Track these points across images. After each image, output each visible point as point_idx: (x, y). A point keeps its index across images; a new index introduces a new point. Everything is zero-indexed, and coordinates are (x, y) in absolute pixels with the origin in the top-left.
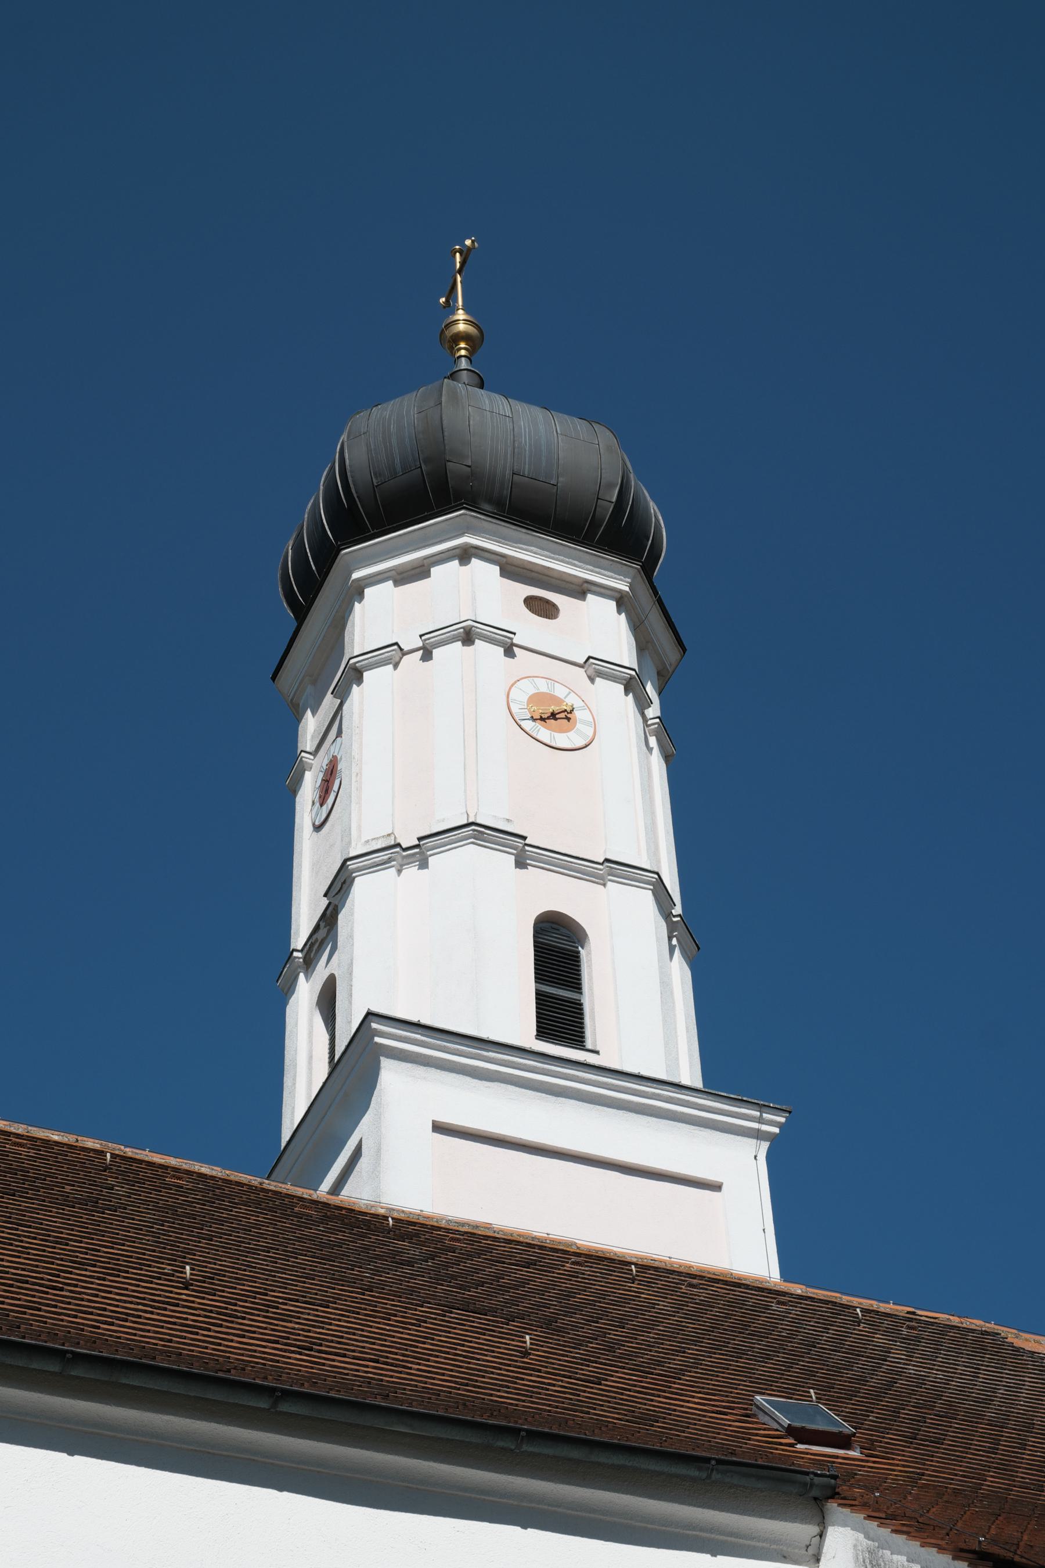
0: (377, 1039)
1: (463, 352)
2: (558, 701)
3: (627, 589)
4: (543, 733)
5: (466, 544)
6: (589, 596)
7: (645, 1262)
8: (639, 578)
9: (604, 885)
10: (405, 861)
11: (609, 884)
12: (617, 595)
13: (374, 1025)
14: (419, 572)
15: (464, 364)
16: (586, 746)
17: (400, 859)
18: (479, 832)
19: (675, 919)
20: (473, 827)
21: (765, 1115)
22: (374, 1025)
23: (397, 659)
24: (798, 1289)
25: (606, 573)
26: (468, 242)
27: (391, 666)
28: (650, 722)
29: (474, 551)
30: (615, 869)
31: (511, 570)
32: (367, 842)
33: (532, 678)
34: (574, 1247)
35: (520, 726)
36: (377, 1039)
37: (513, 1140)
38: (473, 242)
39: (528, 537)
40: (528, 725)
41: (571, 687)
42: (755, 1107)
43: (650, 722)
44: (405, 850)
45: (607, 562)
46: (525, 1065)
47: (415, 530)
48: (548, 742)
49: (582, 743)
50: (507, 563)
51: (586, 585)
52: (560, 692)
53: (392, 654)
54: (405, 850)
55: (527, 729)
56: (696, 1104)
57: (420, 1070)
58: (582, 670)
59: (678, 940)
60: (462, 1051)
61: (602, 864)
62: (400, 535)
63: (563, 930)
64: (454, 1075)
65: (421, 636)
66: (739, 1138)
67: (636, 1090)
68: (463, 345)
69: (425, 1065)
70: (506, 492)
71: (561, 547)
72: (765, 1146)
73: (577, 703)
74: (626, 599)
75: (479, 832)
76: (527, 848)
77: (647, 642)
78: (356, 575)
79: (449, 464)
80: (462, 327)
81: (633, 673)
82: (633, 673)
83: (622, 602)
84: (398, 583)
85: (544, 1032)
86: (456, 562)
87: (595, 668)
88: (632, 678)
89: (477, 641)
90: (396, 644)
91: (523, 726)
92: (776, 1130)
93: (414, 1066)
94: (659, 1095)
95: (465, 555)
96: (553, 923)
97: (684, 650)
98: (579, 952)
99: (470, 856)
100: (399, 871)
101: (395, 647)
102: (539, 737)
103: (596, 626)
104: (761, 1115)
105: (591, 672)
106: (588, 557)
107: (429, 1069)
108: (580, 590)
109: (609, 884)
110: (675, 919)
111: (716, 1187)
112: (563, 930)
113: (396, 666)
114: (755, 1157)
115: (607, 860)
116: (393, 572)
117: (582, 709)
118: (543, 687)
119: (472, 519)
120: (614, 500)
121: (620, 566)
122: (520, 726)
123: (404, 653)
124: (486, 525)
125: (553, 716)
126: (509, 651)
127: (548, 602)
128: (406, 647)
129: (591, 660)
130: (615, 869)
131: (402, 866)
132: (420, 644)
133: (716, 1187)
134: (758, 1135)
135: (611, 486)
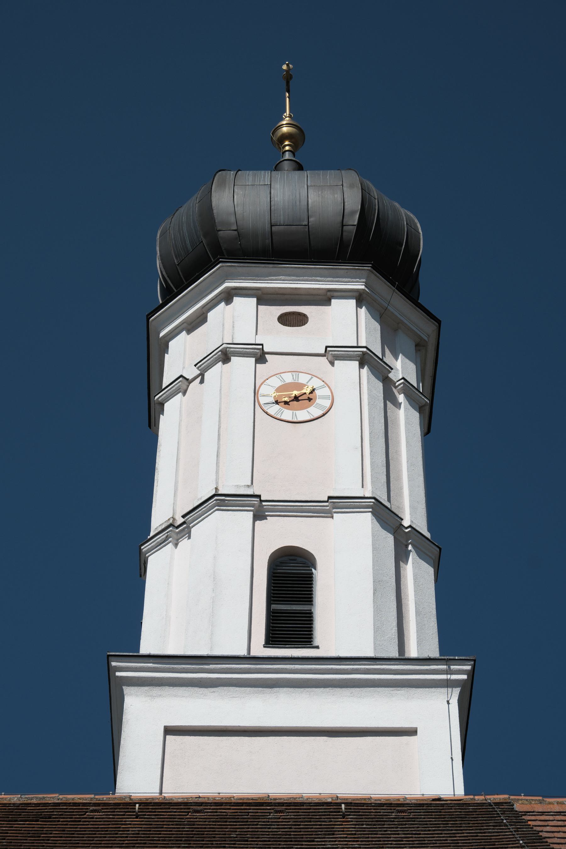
0: (118, 674)
1: (287, 148)
2: (301, 386)
3: (363, 287)
4: (287, 414)
5: (227, 288)
6: (333, 301)
7: (350, 801)
8: (373, 276)
9: (332, 517)
10: (179, 536)
11: (335, 515)
12: (356, 294)
13: (114, 664)
14: (199, 320)
15: (287, 156)
16: (324, 415)
17: (175, 536)
18: (220, 501)
19: (407, 531)
20: (216, 498)
21: (452, 667)
22: (114, 664)
23: (185, 387)
24: (479, 798)
25: (344, 279)
26: (285, 67)
27: (180, 394)
28: (397, 384)
29: (234, 291)
30: (338, 504)
31: (265, 298)
32: (156, 529)
33: (276, 376)
34: (206, 799)
35: (266, 413)
36: (118, 674)
37: (234, 729)
38: (288, 65)
39: (275, 269)
40: (274, 409)
41: (313, 375)
42: (444, 662)
43: (397, 384)
44: (178, 527)
45: (343, 271)
46: (241, 669)
47: (192, 289)
48: (290, 419)
49: (320, 413)
50: (263, 294)
51: (329, 293)
52: (303, 379)
53: (183, 384)
54: (178, 527)
55: (272, 413)
56: (391, 670)
57: (156, 691)
58: (325, 358)
59: (414, 546)
60: (188, 668)
61: (327, 502)
62: (183, 296)
63: (299, 559)
64: (184, 688)
65: (195, 365)
66: (433, 690)
67: (337, 669)
68: (287, 143)
69: (159, 686)
70: (268, 241)
71: (304, 270)
72: (456, 692)
73: (315, 383)
74: (364, 295)
75: (220, 501)
76: (264, 503)
77: (398, 324)
78: (161, 335)
79: (220, 232)
80: (285, 129)
81: (365, 350)
82: (365, 350)
83: (361, 299)
84: (189, 332)
85: (272, 639)
86: (223, 304)
87: (333, 354)
88: (364, 353)
89: (232, 358)
90: (181, 376)
91: (269, 411)
92: (465, 677)
93: (151, 688)
94: (357, 669)
95: (228, 297)
96: (291, 555)
97: (439, 322)
98: (312, 573)
99: (217, 519)
100: (176, 545)
101: (181, 379)
102: (283, 417)
103: (345, 321)
104: (449, 668)
105: (330, 358)
106: (326, 272)
107: (164, 688)
108: (324, 299)
109: (335, 515)
110: (407, 531)
111: (412, 732)
112: (299, 559)
113: (184, 393)
114: (448, 702)
115: (330, 498)
116: (185, 324)
117: (322, 387)
118: (288, 378)
119: (229, 268)
120: (356, 223)
121: (353, 271)
122: (266, 413)
123: (189, 382)
124: (240, 269)
125: (296, 399)
126: (261, 357)
127: (300, 314)
128: (190, 377)
129: (328, 349)
130: (338, 504)
131: (178, 540)
132: (199, 372)
133: (412, 732)
134: (448, 684)
135: (353, 213)
